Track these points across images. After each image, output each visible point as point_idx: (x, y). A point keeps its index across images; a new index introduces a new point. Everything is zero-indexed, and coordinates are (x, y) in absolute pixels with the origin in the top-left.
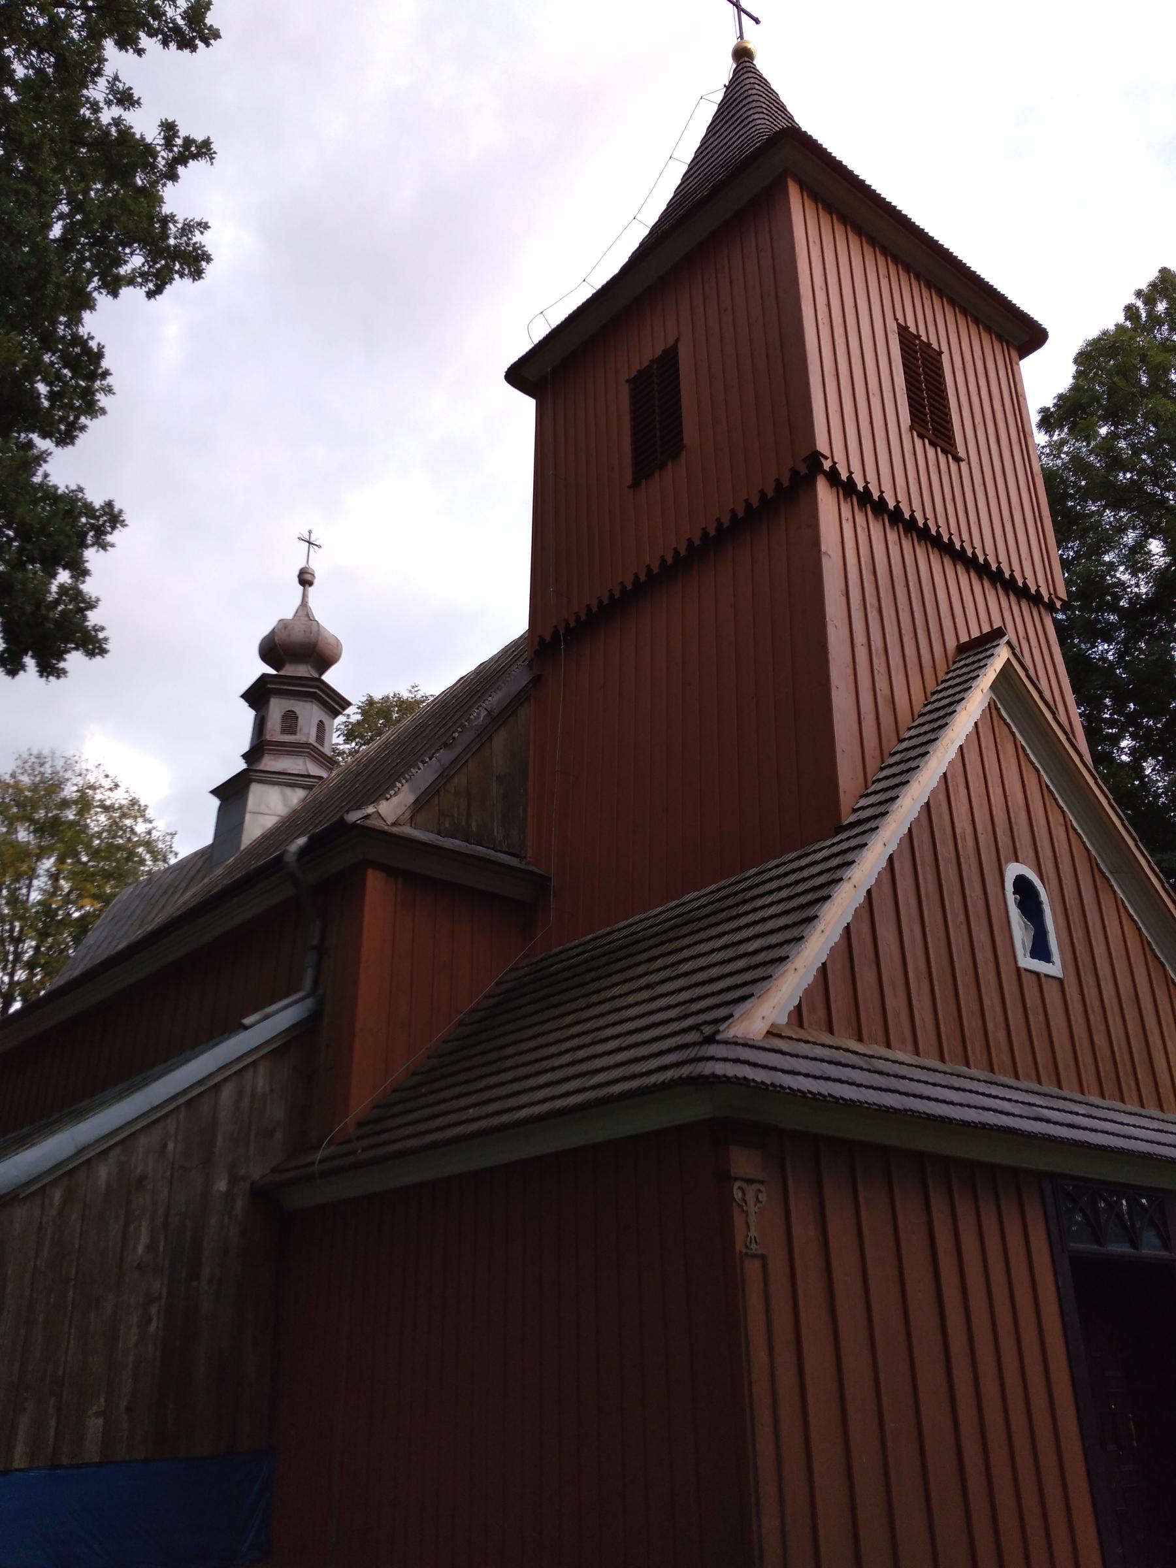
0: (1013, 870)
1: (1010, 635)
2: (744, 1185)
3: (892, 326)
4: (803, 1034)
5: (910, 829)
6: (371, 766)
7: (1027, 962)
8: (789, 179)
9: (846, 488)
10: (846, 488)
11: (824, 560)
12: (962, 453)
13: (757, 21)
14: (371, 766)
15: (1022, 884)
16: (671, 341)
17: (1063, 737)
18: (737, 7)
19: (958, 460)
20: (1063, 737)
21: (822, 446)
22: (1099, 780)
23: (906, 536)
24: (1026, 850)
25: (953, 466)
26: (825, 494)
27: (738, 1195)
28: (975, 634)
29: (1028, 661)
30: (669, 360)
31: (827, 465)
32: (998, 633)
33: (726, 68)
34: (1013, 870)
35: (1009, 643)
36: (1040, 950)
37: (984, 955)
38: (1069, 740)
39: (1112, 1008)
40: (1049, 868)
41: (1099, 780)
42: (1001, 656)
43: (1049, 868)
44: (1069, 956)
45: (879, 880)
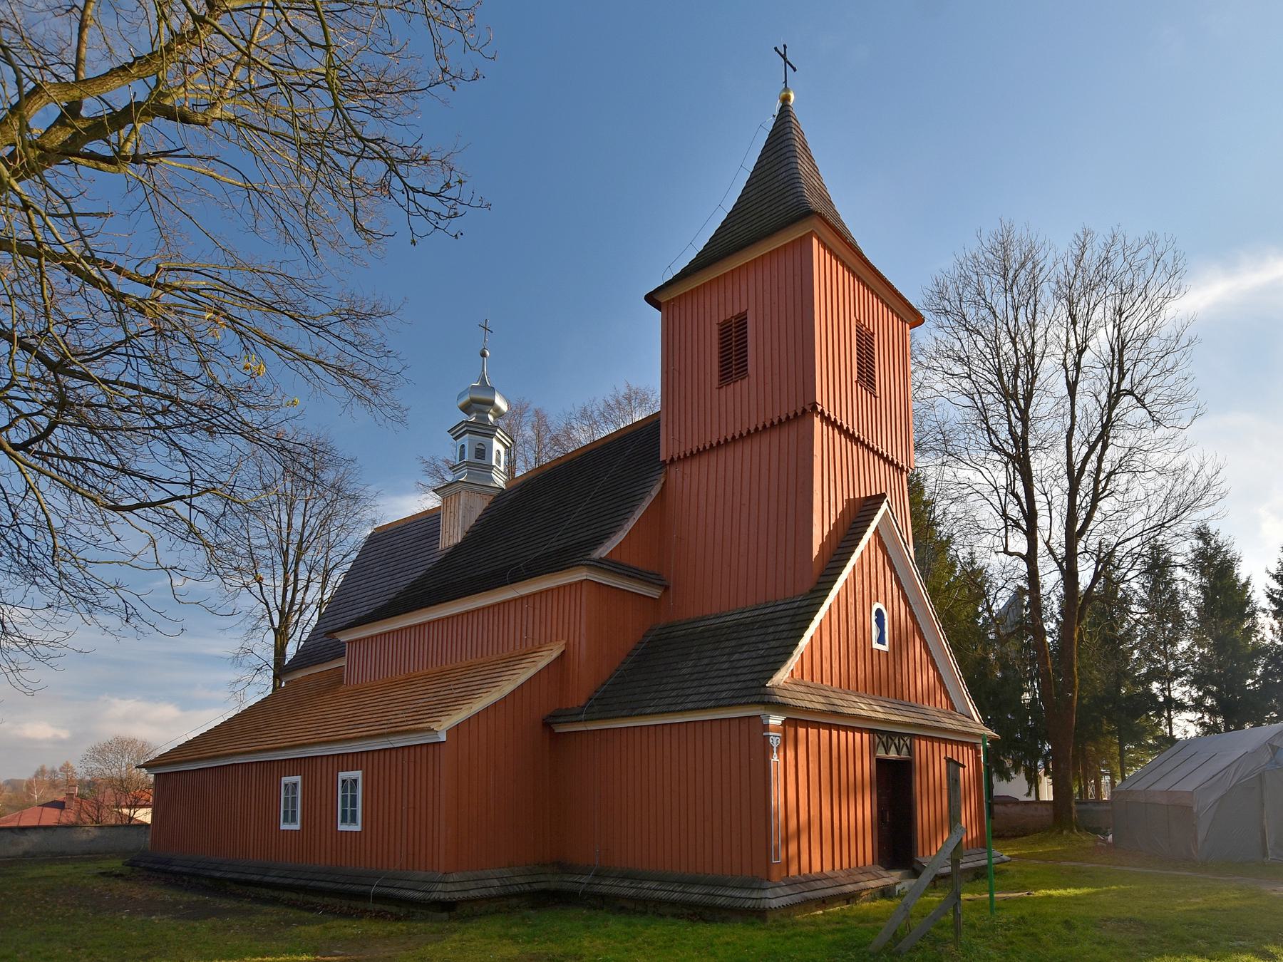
0: (876, 606)
1: (888, 498)
4: (881, 698)
6: (722, 620)
7: (876, 646)
9: (826, 420)
10: (826, 420)
11: (815, 458)
12: (878, 395)
13: (795, 70)
14: (722, 620)
15: (879, 612)
16: (743, 310)
17: (903, 544)
18: (785, 59)
19: (876, 397)
21: (818, 400)
24: (881, 597)
25: (873, 398)
26: (817, 420)
27: (771, 741)
28: (874, 494)
29: (894, 510)
30: (741, 320)
31: (819, 408)
33: (779, 104)
34: (876, 606)
36: (881, 640)
37: (860, 636)
44: (892, 642)
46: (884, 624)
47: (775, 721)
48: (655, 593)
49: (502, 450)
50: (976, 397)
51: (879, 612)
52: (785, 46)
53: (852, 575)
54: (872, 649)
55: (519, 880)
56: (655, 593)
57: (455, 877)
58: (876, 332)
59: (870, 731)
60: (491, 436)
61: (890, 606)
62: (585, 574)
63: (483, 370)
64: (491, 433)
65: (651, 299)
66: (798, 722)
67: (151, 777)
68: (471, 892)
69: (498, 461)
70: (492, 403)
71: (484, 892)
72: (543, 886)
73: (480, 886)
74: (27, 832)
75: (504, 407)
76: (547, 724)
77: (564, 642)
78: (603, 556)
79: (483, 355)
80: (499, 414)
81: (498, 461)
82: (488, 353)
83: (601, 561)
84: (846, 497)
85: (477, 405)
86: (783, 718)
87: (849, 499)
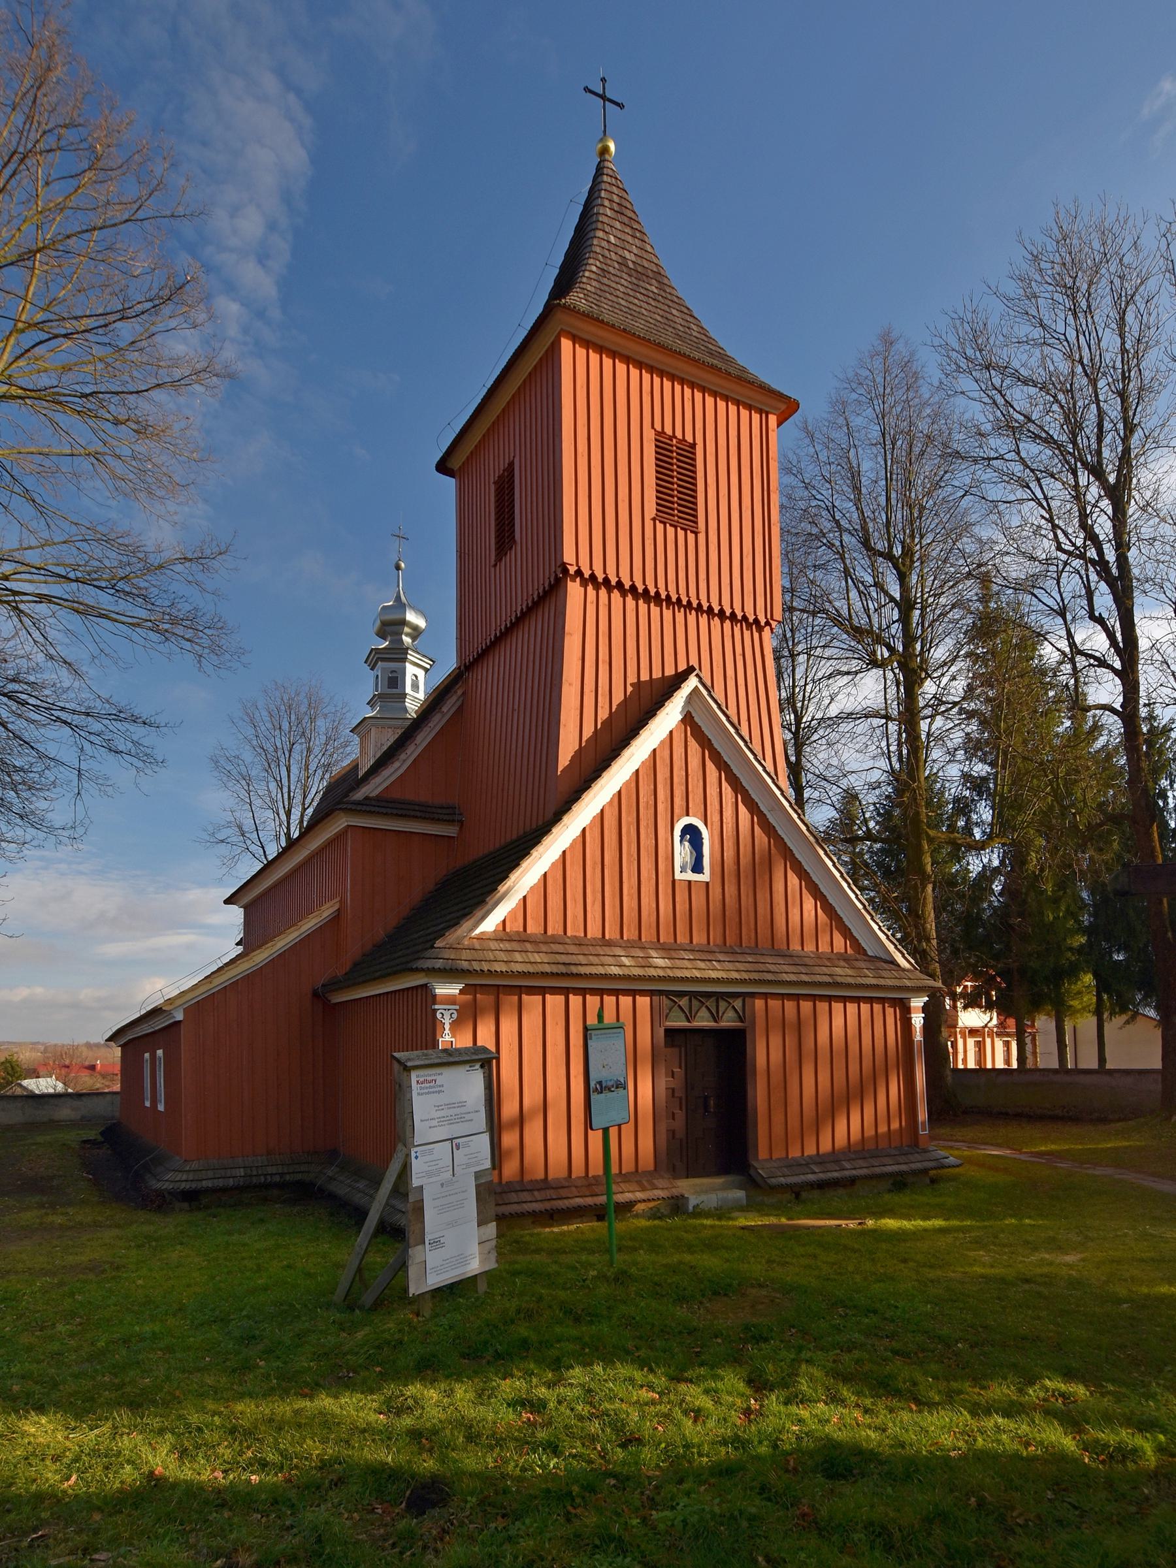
2: (443, 1011)
3: (649, 435)
5: (602, 811)
8: (562, 339)
17: (732, 730)
20: (769, 781)
22: (907, 955)
23: (747, 629)
32: (690, 670)
35: (697, 675)
36: (697, 868)
38: (799, 818)
39: (748, 911)
40: (714, 817)
41: (907, 955)
42: (692, 683)
43: (714, 817)
44: (718, 869)
45: (572, 845)
46: (702, 844)
47: (447, 989)
48: (451, 831)
49: (421, 674)
50: (1033, 485)
51: (691, 832)
52: (603, 80)
53: (633, 785)
54: (674, 881)
55: (270, 1170)
56: (451, 831)
57: (195, 1165)
58: (699, 441)
59: (651, 993)
60: (404, 660)
61: (716, 818)
62: (344, 819)
63: (398, 586)
64: (403, 656)
65: (443, 467)
66: (501, 988)
67: (118, 1052)
68: (204, 1182)
69: (415, 687)
70: (403, 622)
71: (220, 1183)
72: (299, 1177)
73: (217, 1176)
74: (83, 1098)
75: (421, 623)
76: (319, 996)
77: (338, 899)
78: (373, 794)
79: (398, 568)
80: (416, 632)
81: (415, 687)
82: (403, 565)
83: (358, 803)
84: (632, 679)
85: (391, 626)
86: (461, 986)
87: (638, 685)
